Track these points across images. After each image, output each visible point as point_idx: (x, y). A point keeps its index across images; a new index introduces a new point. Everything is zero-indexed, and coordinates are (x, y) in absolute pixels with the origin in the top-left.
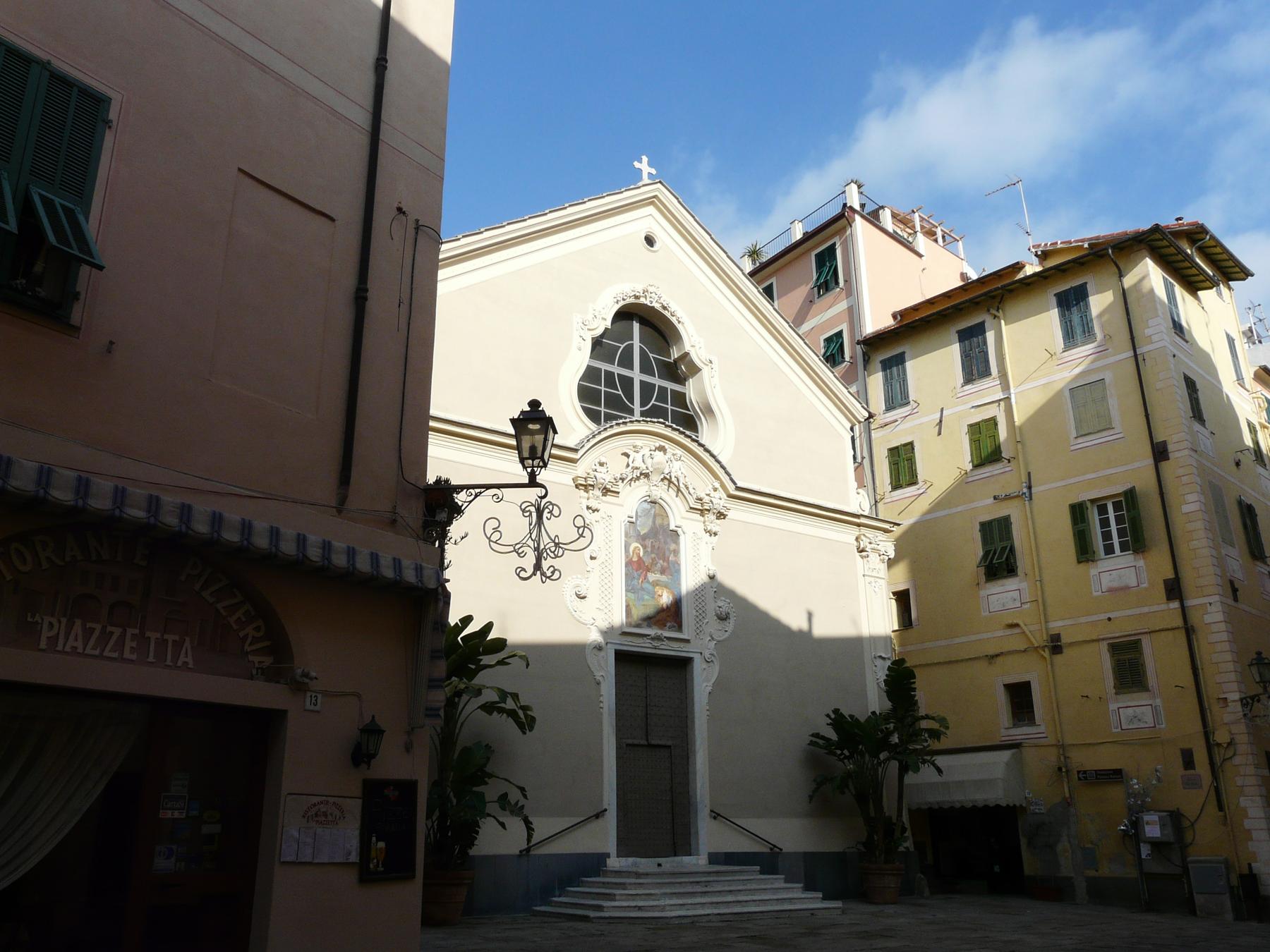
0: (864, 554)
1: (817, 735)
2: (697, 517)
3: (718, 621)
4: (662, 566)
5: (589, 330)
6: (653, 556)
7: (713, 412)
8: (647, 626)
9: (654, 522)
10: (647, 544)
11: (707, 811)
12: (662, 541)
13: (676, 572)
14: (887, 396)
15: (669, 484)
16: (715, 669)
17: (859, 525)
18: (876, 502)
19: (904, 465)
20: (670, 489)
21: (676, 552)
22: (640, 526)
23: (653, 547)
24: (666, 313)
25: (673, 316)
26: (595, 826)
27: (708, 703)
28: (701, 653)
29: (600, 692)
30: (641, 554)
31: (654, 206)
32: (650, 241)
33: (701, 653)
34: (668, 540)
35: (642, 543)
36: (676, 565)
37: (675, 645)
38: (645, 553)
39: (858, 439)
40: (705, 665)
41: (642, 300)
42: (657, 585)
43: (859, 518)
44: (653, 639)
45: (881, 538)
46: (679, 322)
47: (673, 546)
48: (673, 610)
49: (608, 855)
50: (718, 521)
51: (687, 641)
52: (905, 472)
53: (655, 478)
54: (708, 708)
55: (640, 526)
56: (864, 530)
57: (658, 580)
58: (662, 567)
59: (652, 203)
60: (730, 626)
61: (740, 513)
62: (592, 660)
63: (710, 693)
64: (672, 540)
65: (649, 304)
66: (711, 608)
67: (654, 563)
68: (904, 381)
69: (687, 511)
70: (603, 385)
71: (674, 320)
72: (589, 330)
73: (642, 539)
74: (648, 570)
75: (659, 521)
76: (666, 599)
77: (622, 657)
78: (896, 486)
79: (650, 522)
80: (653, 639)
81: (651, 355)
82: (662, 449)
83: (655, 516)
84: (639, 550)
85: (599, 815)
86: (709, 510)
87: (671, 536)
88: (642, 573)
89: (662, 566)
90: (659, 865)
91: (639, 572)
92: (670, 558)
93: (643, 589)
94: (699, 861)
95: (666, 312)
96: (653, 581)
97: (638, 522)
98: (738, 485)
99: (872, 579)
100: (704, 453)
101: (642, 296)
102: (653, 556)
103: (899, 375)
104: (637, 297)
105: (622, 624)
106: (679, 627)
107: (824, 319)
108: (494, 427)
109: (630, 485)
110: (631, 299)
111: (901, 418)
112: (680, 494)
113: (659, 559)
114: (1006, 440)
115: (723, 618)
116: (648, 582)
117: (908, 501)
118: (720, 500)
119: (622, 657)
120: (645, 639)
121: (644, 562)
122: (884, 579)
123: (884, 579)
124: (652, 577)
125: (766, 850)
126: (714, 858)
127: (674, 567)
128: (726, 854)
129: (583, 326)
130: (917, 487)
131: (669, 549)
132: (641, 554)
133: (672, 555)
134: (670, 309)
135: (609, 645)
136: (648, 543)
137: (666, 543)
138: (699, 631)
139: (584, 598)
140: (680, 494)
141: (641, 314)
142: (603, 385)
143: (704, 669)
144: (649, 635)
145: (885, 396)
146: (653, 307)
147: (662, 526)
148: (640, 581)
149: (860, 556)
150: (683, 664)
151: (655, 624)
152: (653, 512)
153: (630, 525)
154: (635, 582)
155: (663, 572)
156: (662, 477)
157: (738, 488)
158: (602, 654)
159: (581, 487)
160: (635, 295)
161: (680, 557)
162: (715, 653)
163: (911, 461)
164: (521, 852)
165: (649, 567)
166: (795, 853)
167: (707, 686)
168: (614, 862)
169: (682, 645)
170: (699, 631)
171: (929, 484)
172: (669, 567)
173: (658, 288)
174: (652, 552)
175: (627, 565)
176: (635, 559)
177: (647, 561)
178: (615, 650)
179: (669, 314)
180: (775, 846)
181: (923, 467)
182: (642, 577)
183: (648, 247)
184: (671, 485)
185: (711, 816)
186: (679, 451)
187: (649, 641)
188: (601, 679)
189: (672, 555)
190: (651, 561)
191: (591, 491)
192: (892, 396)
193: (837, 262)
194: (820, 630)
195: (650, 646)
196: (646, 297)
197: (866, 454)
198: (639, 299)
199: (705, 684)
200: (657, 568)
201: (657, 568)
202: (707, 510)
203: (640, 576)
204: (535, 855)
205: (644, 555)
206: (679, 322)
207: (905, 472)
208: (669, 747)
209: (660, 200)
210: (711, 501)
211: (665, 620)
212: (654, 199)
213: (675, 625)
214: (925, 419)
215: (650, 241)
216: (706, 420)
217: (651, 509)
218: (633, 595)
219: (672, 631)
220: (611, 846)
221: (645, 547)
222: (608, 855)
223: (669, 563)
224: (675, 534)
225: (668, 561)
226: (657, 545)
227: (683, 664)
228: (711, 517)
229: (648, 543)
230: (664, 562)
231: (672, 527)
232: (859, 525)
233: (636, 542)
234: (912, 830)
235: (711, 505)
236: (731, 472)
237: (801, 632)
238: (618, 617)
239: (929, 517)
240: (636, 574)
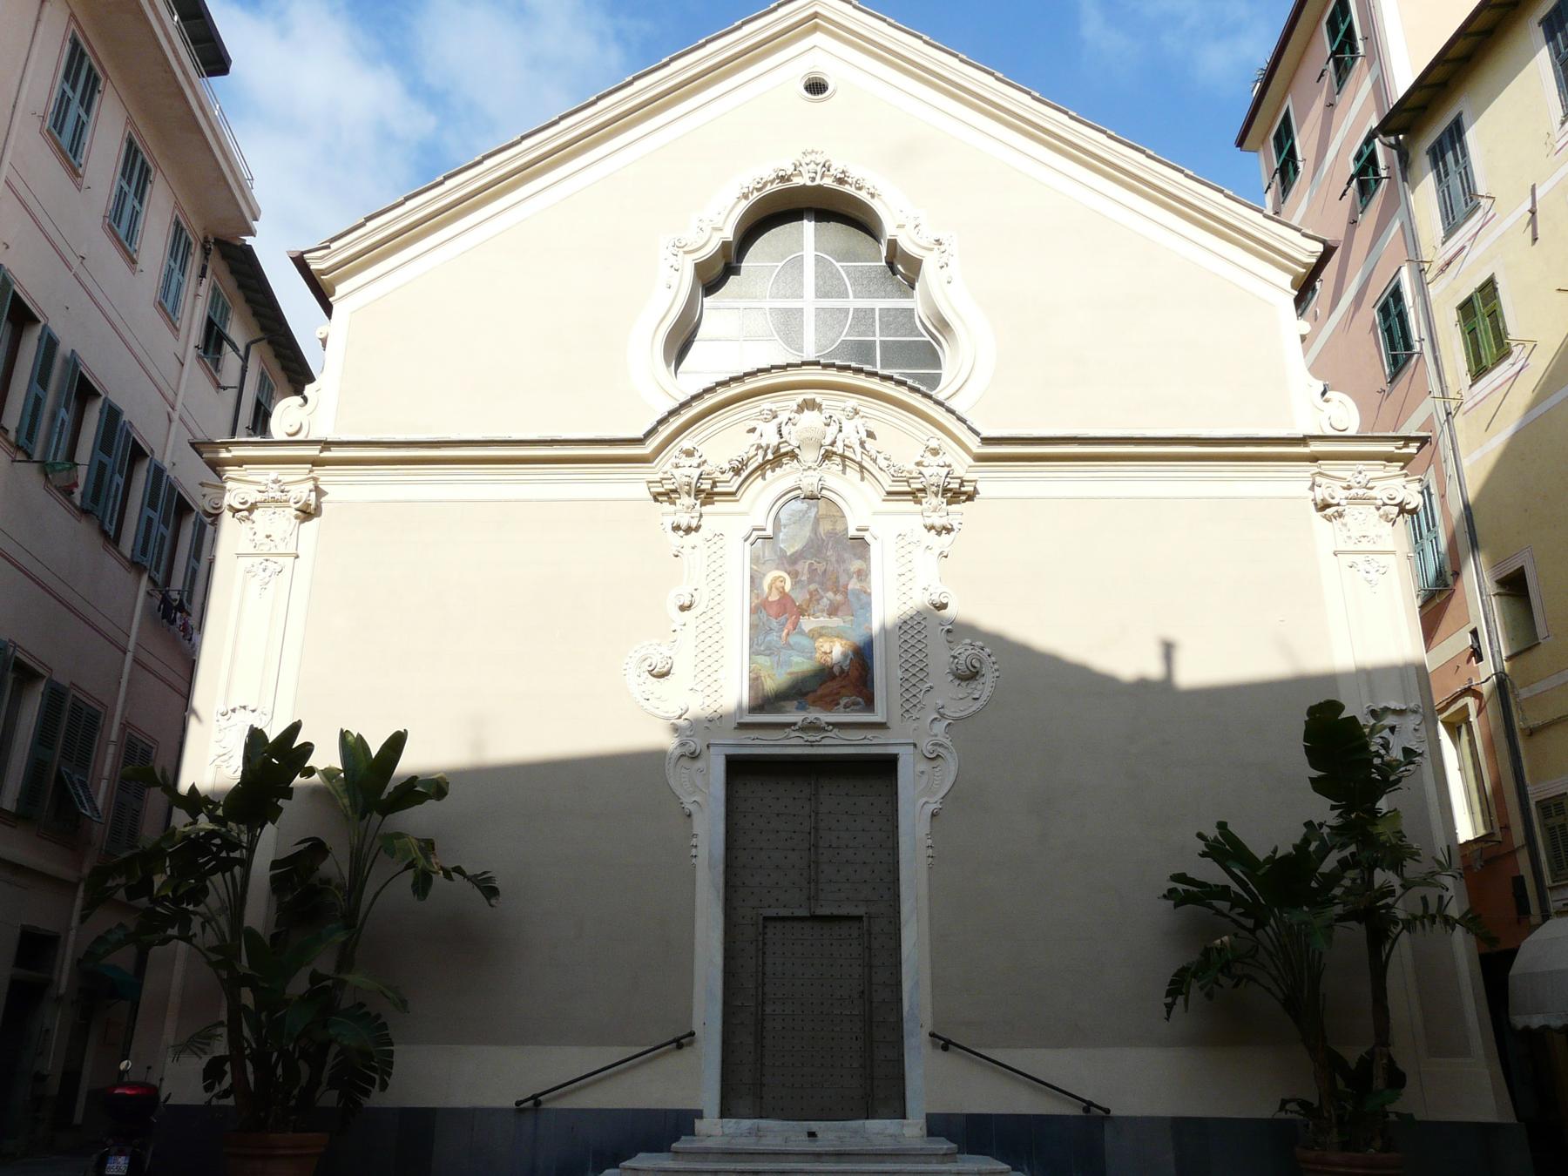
0: (1329, 511)
1: (1180, 878)
2: (910, 506)
3: (957, 682)
4: (831, 601)
5: (686, 253)
6: (812, 587)
7: (949, 325)
8: (797, 708)
9: (815, 530)
10: (800, 570)
11: (924, 1035)
12: (834, 559)
13: (862, 608)
14: (1444, 210)
15: (843, 461)
16: (948, 772)
17: (1314, 458)
18: (1448, 414)
19: (1484, 325)
20: (848, 469)
21: (863, 575)
22: (783, 541)
23: (812, 571)
24: (846, 189)
25: (860, 189)
26: (675, 1061)
27: (930, 835)
28: (915, 745)
29: (691, 827)
30: (788, 587)
31: (822, 32)
32: (816, 87)
33: (915, 745)
34: (846, 555)
35: (789, 569)
36: (863, 597)
37: (856, 736)
38: (794, 585)
39: (1412, 310)
40: (923, 766)
41: (798, 181)
42: (821, 635)
43: (1306, 445)
44: (803, 729)
45: (1371, 475)
46: (873, 195)
47: (856, 565)
48: (854, 674)
49: (699, 1114)
50: (954, 507)
51: (881, 726)
52: (1489, 342)
53: (809, 456)
54: (930, 842)
55: (783, 541)
56: (1325, 466)
57: (822, 628)
58: (830, 605)
59: (816, 28)
60: (984, 688)
61: (994, 484)
62: (681, 781)
63: (933, 815)
64: (855, 555)
65: (809, 183)
66: (940, 660)
67: (814, 598)
68: (1465, 168)
69: (884, 500)
70: (878, 344)
71: (863, 195)
72: (686, 253)
73: (790, 562)
74: (802, 612)
75: (825, 527)
76: (836, 651)
77: (738, 768)
78: (1479, 370)
79: (807, 532)
80: (803, 729)
81: (838, 265)
82: (810, 405)
83: (817, 520)
84: (784, 581)
85: (682, 1041)
86: (923, 490)
87: (853, 547)
88: (787, 619)
89: (831, 601)
90: (812, 1135)
91: (782, 619)
92: (850, 587)
93: (789, 646)
94: (912, 1130)
95: (847, 186)
96: (810, 631)
97: (781, 536)
98: (985, 434)
99: (1360, 559)
100: (898, 388)
101: (796, 175)
102: (812, 587)
103: (1457, 162)
104: (782, 179)
105: (740, 707)
106: (869, 704)
107: (1350, 123)
108: (485, 436)
109: (764, 478)
110: (774, 186)
111: (1470, 239)
112: (866, 474)
113: (826, 590)
114: (1448, 151)
115: (970, 676)
116: (802, 633)
117: (1499, 395)
118: (962, 466)
119: (738, 768)
120: (787, 730)
121: (793, 601)
122: (1393, 552)
123: (1393, 552)
124: (808, 623)
125: (1079, 1112)
126: (938, 1125)
127: (859, 599)
128: (971, 1118)
129: (675, 250)
130: (1511, 360)
131: (846, 571)
132: (788, 587)
133: (854, 580)
134: (850, 180)
135: (711, 748)
136: (803, 567)
137: (841, 560)
138: (910, 706)
139: (666, 674)
140: (866, 474)
141: (814, 205)
142: (878, 344)
143: (922, 772)
144: (795, 724)
145: (1441, 211)
146: (819, 186)
147: (832, 534)
148: (784, 634)
149: (1325, 517)
150: (885, 767)
151: (814, 703)
152: (813, 515)
153: (763, 544)
154: (773, 637)
155: (833, 611)
156: (823, 451)
157: (987, 441)
158: (699, 764)
159: (660, 499)
160: (778, 177)
161: (869, 583)
162: (947, 742)
163: (1495, 316)
164: (518, 1104)
165: (804, 607)
166: (1163, 1119)
167: (927, 802)
168: (713, 1129)
169: (870, 734)
170: (910, 706)
171: (1530, 346)
172: (846, 601)
173: (822, 152)
174: (810, 581)
175: (754, 611)
176: (774, 597)
177: (800, 597)
178: (727, 756)
179: (853, 189)
180: (1090, 1104)
181: (1516, 323)
182: (789, 625)
183: (820, 96)
184: (848, 463)
185: (934, 1045)
186: (853, 401)
187: (797, 734)
188: (692, 808)
189: (854, 580)
190: (808, 597)
191: (677, 501)
192: (1451, 206)
193: (1351, 16)
194: (1193, 673)
195: (801, 742)
196: (801, 173)
197: (1424, 335)
198: (789, 180)
199: (924, 800)
200: (820, 607)
201: (820, 607)
202: (920, 490)
203: (784, 625)
204: (549, 1109)
205: (792, 589)
206: (873, 195)
207: (1489, 342)
208: (860, 918)
209: (826, 17)
210: (920, 473)
211: (838, 693)
212: (816, 20)
213: (860, 700)
214: (1510, 221)
215: (816, 87)
216: (945, 338)
217: (809, 509)
218: (767, 658)
219: (853, 711)
220: (708, 1096)
221: (794, 575)
222: (699, 1114)
223: (847, 593)
224: (860, 545)
225: (845, 593)
226: (821, 568)
227: (885, 767)
228: (932, 501)
229: (803, 567)
230: (835, 594)
231: (852, 532)
232: (1314, 458)
233: (777, 569)
234: (232, 1074)
235: (922, 479)
236: (965, 416)
237: (1142, 686)
238: (732, 693)
239: (1537, 412)
240: (774, 623)
